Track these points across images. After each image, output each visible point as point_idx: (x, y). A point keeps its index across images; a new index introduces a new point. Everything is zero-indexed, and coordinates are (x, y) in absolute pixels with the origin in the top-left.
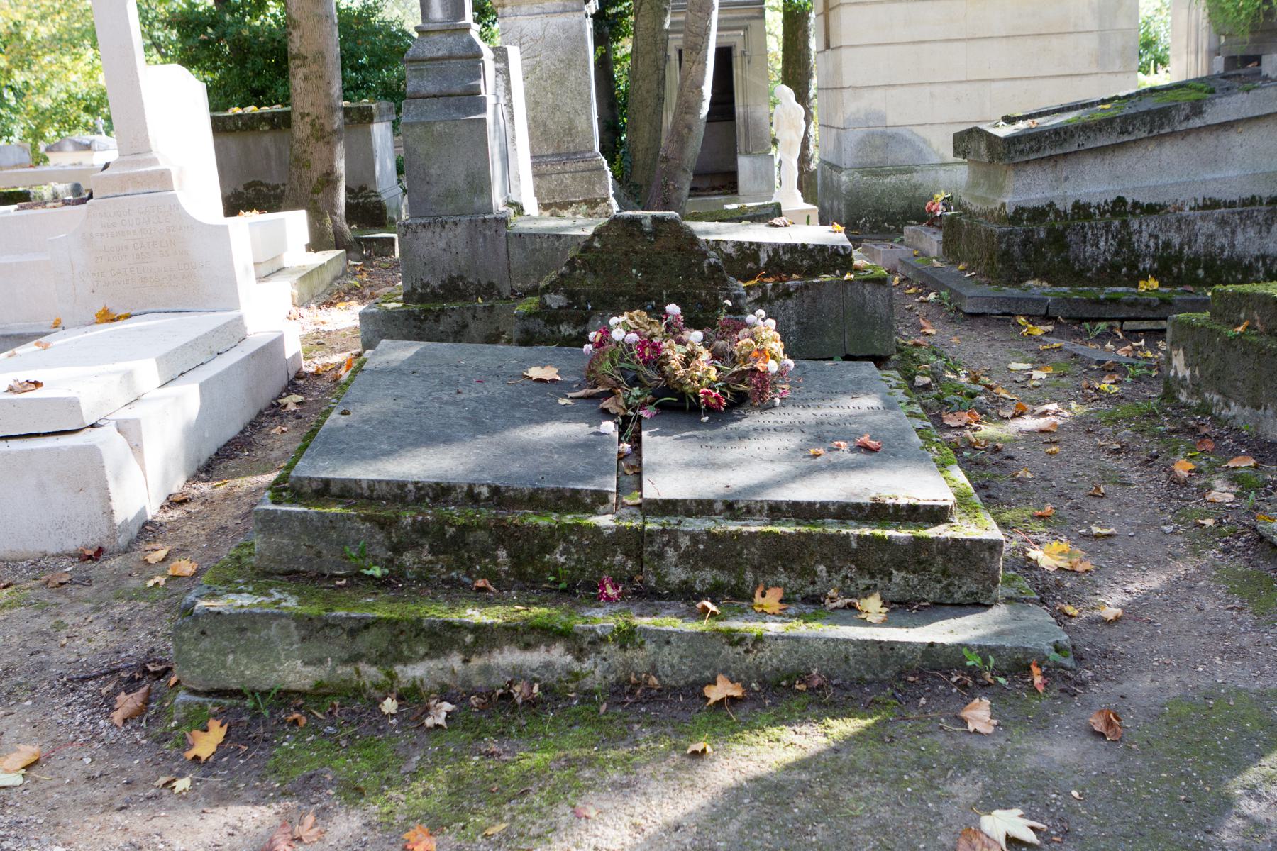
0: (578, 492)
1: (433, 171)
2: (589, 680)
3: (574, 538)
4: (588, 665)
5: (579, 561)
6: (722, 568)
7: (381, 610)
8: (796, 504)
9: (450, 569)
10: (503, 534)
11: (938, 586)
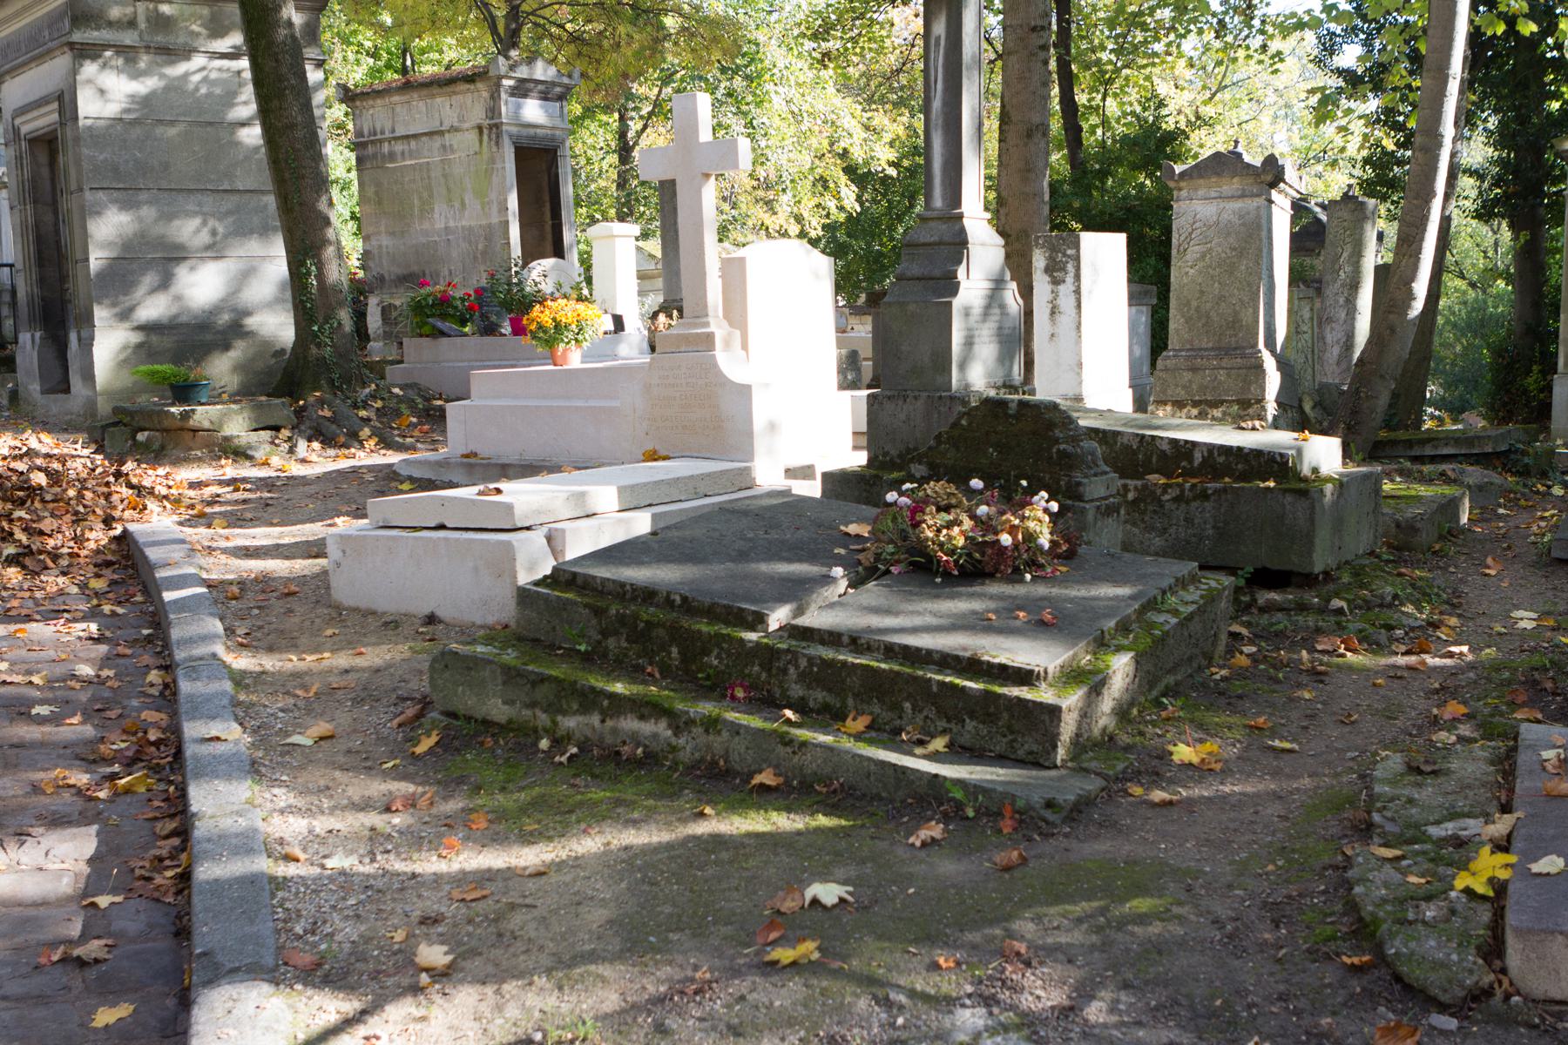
0: (742, 610)
1: (903, 348)
2: (682, 754)
3: (725, 646)
4: (682, 741)
5: (727, 666)
6: (830, 690)
7: (558, 671)
8: (906, 648)
9: (639, 657)
10: (677, 634)
11: (1004, 740)
